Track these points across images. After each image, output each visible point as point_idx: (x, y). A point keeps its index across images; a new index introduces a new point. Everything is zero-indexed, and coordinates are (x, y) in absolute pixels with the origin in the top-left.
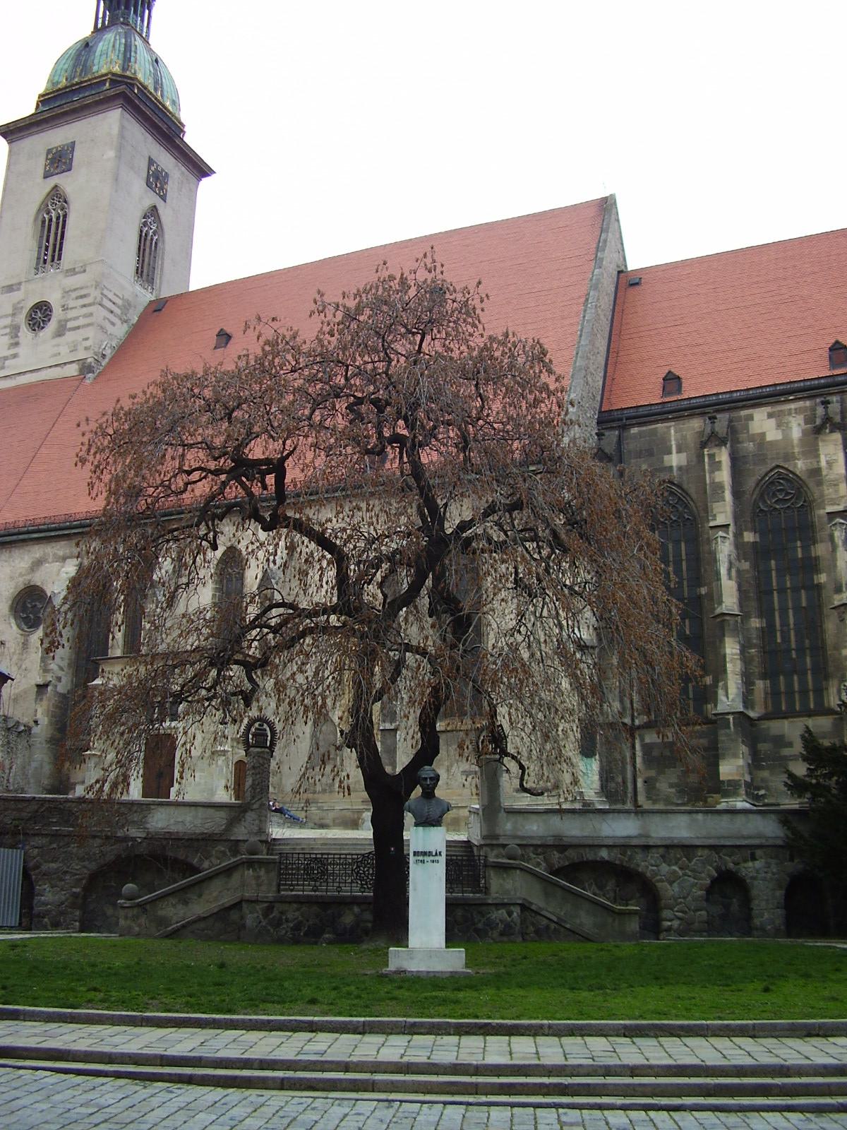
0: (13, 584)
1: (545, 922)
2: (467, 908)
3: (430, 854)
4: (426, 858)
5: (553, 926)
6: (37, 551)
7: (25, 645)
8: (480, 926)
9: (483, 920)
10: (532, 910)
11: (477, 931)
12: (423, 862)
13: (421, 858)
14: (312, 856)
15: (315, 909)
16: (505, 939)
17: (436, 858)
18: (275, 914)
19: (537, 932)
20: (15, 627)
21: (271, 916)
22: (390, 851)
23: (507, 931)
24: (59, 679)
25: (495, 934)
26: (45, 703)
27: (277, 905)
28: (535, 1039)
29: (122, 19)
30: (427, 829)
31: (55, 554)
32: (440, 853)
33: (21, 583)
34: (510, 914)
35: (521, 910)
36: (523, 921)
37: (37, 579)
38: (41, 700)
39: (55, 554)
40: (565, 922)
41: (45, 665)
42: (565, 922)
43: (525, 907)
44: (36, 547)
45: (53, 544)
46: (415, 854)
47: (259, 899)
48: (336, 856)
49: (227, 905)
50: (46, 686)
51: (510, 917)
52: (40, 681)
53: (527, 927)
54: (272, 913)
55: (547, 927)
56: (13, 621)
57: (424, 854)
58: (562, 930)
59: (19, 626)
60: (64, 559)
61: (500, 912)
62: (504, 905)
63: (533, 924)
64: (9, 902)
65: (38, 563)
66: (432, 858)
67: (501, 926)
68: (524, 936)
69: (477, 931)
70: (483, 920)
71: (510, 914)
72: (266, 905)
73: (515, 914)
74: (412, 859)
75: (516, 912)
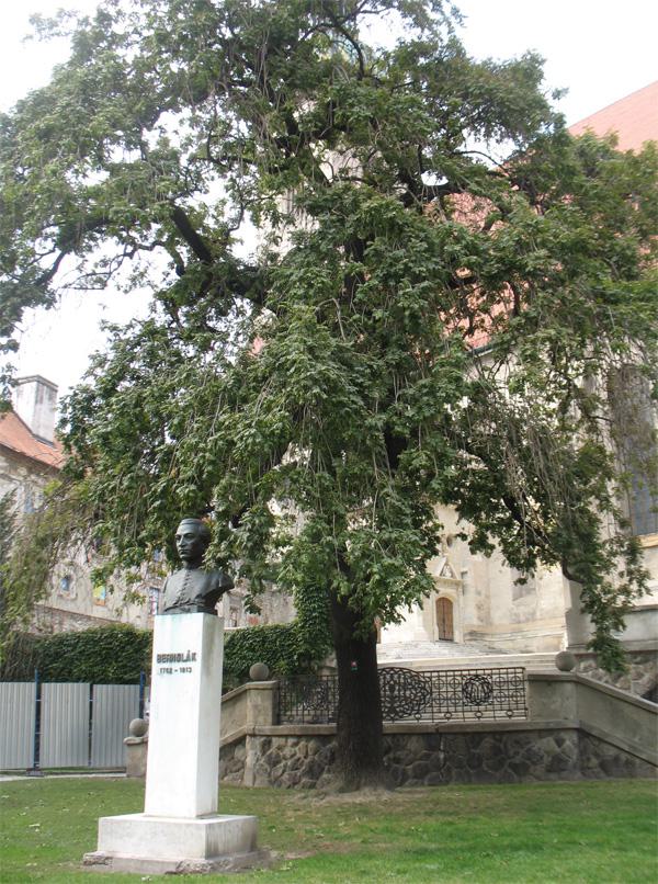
1: (612, 752)
2: (497, 737)
4: (176, 666)
5: (624, 757)
8: (517, 760)
9: (522, 752)
10: (593, 736)
11: (515, 767)
12: (169, 671)
13: (166, 665)
14: (472, 672)
15: (312, 744)
16: (552, 776)
17: (188, 664)
18: (273, 750)
19: (603, 766)
21: (269, 752)
22: (350, 665)
23: (557, 766)
25: (540, 770)
27: (274, 739)
28: (460, 518)
29: (418, 483)
30: (178, 616)
34: (560, 742)
35: (580, 739)
36: (582, 753)
40: (640, 751)
42: (640, 751)
43: (583, 733)
46: (161, 658)
47: (257, 733)
48: (441, 674)
49: (230, 740)
51: (559, 746)
53: (589, 759)
54: (269, 748)
55: (617, 759)
58: (637, 761)
61: (545, 740)
62: (549, 731)
63: (597, 755)
64: (106, 738)
66: (182, 665)
67: (547, 760)
68: (585, 770)
69: (515, 767)
70: (522, 752)
71: (560, 742)
72: (263, 739)
73: (568, 742)
74: (156, 666)
75: (570, 741)
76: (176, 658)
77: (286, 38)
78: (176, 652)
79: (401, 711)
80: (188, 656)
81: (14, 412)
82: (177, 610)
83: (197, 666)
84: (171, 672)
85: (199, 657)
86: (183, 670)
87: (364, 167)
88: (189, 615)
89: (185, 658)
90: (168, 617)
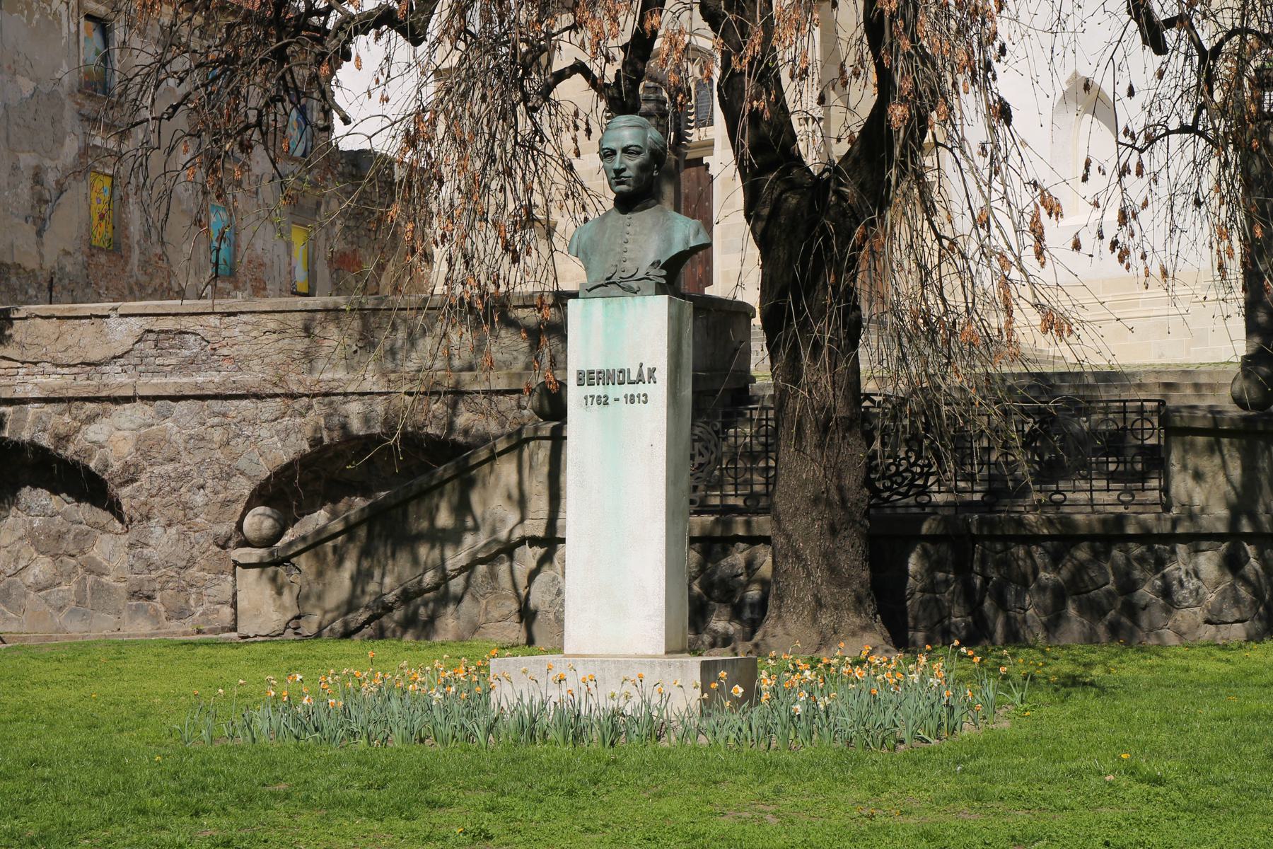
4: (614, 391)
12: (603, 401)
13: (598, 390)
17: (640, 389)
30: (615, 302)
32: (652, 371)
46: (587, 378)
66: (628, 389)
76: (606, 377)
77: (1131, 530)
79: (887, 489)
80: (640, 374)
81: (682, 651)
82: (614, 289)
83: (658, 391)
84: (606, 403)
85: (662, 375)
86: (632, 399)
87: (1137, 20)
88: (638, 299)
89: (634, 377)
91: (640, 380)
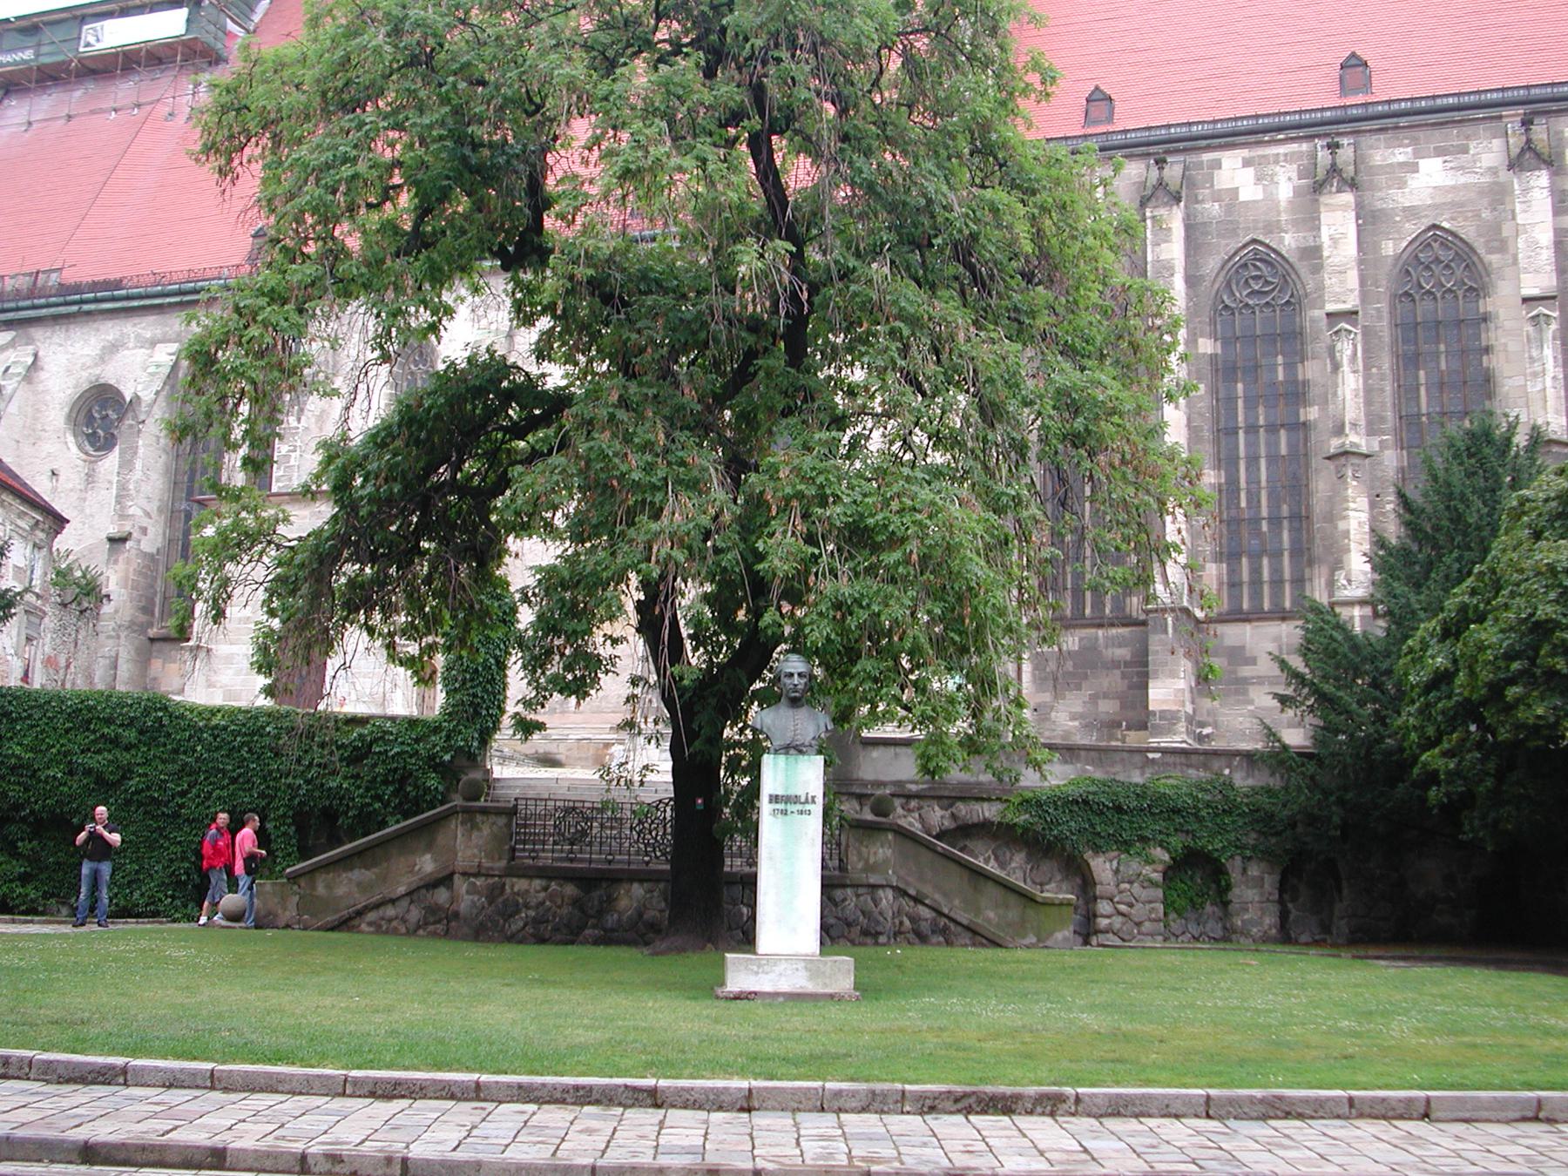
0: (71, 382)
3: (794, 799)
4: (790, 807)
6: (110, 330)
7: (90, 478)
12: (784, 812)
13: (781, 806)
17: (808, 807)
20: (74, 449)
24: (144, 531)
26: (121, 566)
30: (792, 759)
31: (138, 336)
33: (84, 379)
37: (110, 375)
38: (116, 562)
39: (138, 336)
41: (123, 508)
44: (110, 324)
45: (137, 320)
46: (775, 799)
50: (123, 540)
52: (113, 530)
56: (70, 439)
57: (788, 799)
59: (80, 447)
60: (153, 343)
65: (113, 348)
66: (799, 807)
78: (792, 792)
82: (792, 751)
86: (801, 812)
90: (782, 758)
91: (807, 802)
